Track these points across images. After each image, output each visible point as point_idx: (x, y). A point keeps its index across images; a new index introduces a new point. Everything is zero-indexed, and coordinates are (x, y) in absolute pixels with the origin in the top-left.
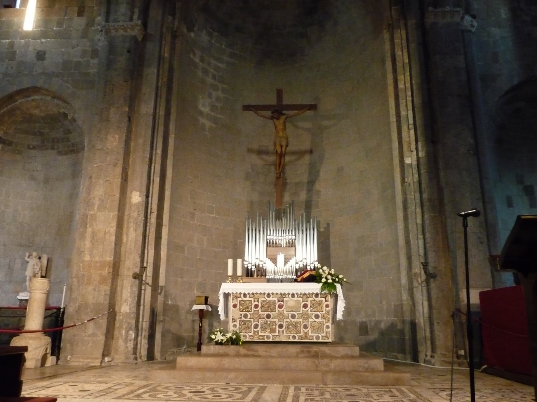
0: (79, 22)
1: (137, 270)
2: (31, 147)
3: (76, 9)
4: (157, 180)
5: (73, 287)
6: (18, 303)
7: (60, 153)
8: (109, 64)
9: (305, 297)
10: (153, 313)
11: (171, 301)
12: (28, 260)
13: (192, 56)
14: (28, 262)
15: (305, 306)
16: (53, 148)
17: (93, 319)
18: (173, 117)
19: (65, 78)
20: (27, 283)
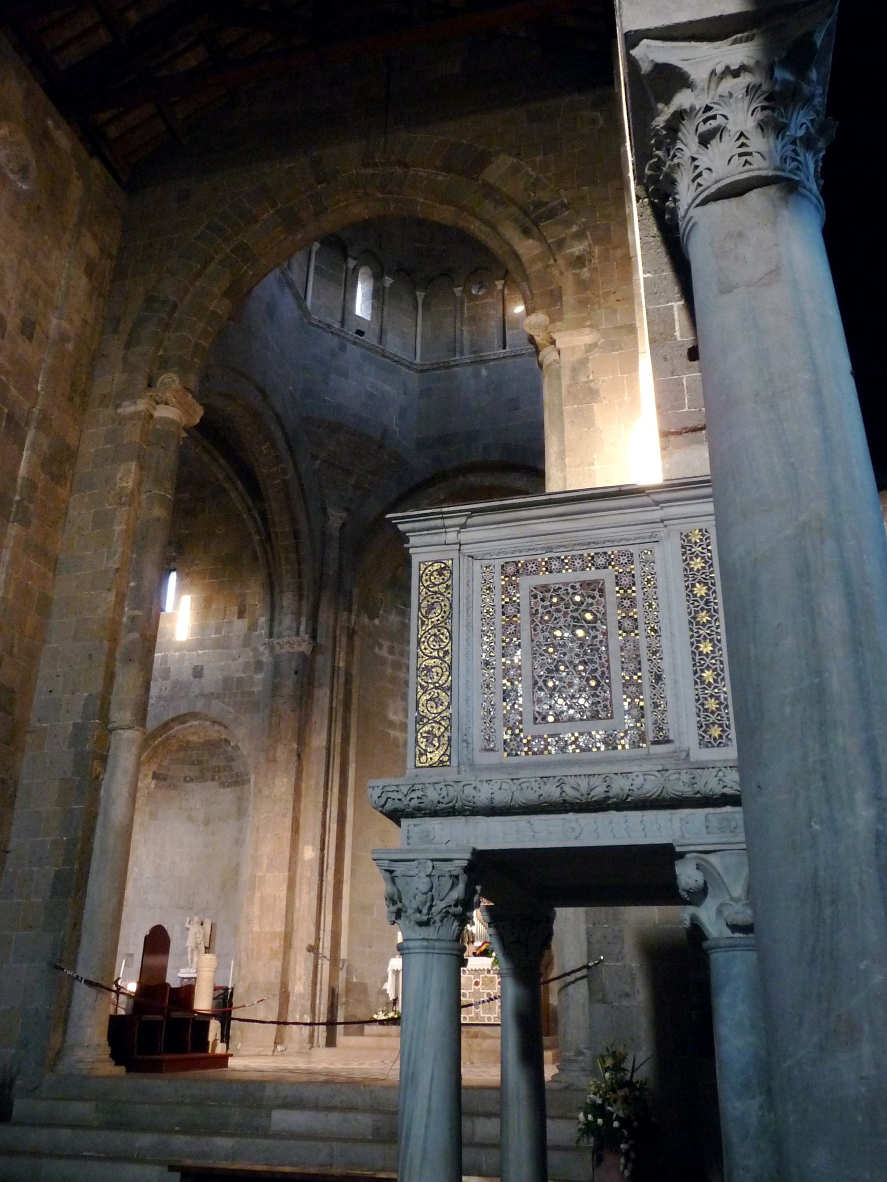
0: (240, 626)
1: (312, 942)
2: (188, 779)
3: (235, 609)
4: (333, 826)
5: (242, 963)
6: (178, 982)
7: (223, 785)
8: (275, 689)
9: (476, 974)
10: (333, 994)
11: (356, 978)
12: (188, 926)
13: (377, 650)
14: (188, 929)
15: (477, 983)
16: (213, 779)
17: (262, 1000)
18: (353, 740)
19: (226, 700)
20: (189, 957)
